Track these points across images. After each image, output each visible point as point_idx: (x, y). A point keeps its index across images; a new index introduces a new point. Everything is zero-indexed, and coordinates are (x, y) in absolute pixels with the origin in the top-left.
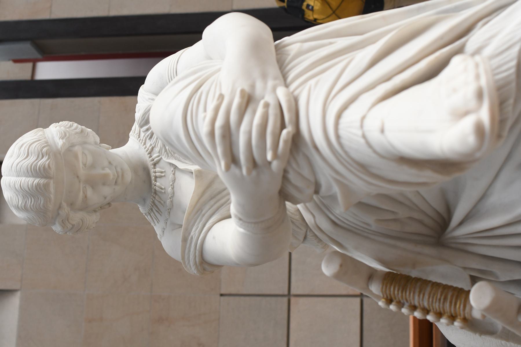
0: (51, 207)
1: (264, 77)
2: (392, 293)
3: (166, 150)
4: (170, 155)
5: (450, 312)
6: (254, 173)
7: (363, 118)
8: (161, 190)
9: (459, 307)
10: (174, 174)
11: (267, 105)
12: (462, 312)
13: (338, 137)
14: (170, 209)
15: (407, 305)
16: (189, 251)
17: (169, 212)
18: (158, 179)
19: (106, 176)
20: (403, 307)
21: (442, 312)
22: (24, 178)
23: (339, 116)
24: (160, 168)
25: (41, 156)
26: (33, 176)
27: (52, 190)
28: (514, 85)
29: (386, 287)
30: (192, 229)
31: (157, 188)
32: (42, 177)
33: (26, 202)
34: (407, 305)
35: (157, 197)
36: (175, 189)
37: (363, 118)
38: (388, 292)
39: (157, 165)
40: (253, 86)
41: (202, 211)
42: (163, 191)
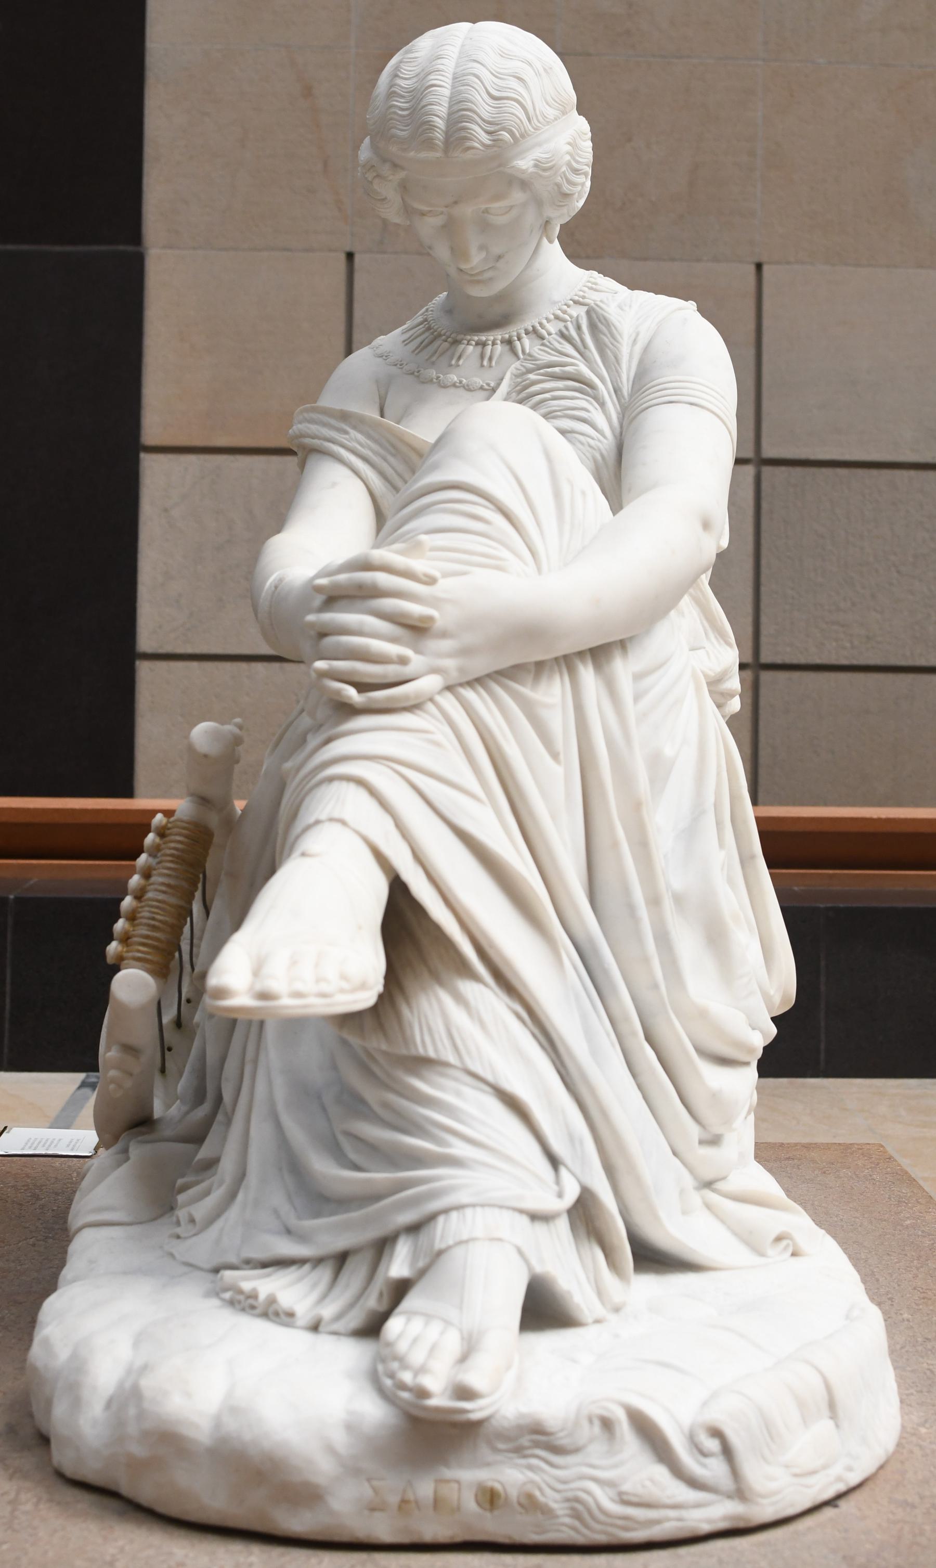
0: (394, 149)
1: (465, 652)
2: (173, 838)
3: (530, 371)
4: (519, 380)
5: (135, 936)
6: (312, 633)
7: (343, 822)
8: (457, 355)
9: (139, 951)
10: (482, 388)
11: (403, 661)
12: (130, 954)
13: (331, 779)
14: (418, 377)
15: (153, 862)
16: (325, 425)
17: (412, 374)
18: (479, 348)
19: (465, 256)
20: (150, 855)
21: (136, 922)
22: (447, 92)
23: (360, 782)
24: (500, 355)
25: (491, 128)
26: (450, 114)
27: (423, 155)
28: (404, 1052)
29: (184, 828)
30: (361, 432)
31: (462, 347)
32: (448, 134)
33: (403, 97)
34: (153, 862)
35: (446, 345)
36: (452, 390)
37: (343, 822)
38: (175, 830)
39: (507, 348)
40: (444, 635)
41: (393, 455)
42: (453, 362)
